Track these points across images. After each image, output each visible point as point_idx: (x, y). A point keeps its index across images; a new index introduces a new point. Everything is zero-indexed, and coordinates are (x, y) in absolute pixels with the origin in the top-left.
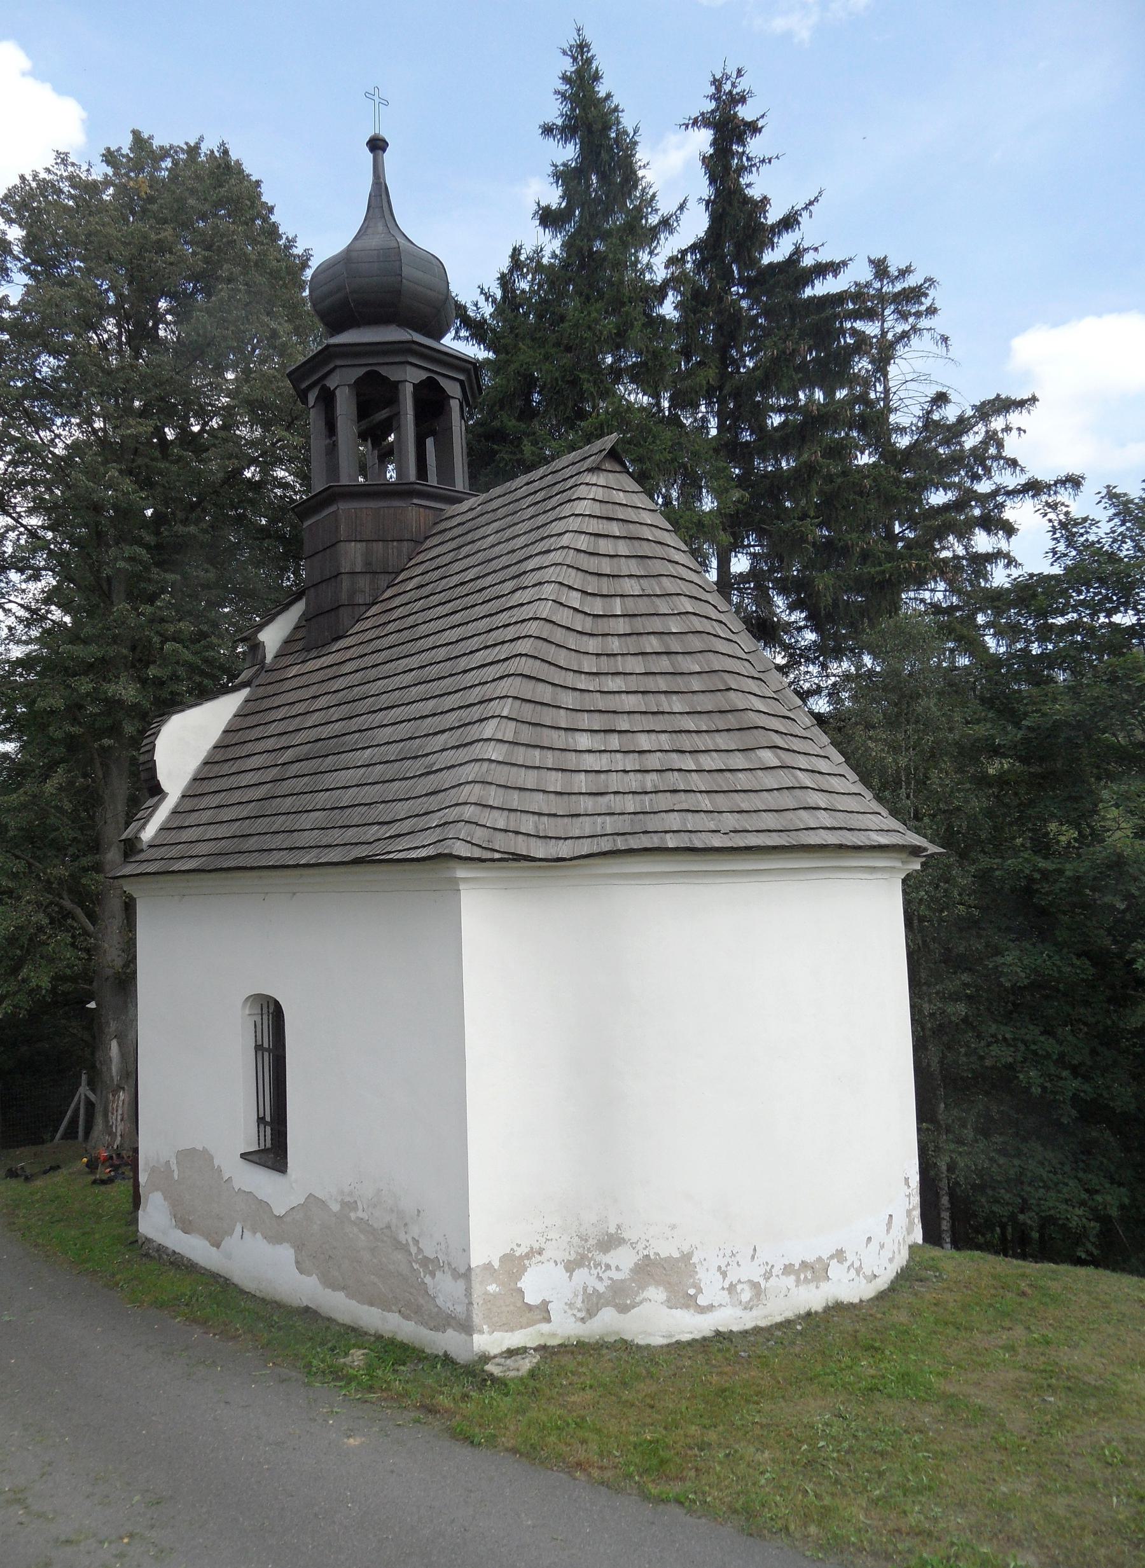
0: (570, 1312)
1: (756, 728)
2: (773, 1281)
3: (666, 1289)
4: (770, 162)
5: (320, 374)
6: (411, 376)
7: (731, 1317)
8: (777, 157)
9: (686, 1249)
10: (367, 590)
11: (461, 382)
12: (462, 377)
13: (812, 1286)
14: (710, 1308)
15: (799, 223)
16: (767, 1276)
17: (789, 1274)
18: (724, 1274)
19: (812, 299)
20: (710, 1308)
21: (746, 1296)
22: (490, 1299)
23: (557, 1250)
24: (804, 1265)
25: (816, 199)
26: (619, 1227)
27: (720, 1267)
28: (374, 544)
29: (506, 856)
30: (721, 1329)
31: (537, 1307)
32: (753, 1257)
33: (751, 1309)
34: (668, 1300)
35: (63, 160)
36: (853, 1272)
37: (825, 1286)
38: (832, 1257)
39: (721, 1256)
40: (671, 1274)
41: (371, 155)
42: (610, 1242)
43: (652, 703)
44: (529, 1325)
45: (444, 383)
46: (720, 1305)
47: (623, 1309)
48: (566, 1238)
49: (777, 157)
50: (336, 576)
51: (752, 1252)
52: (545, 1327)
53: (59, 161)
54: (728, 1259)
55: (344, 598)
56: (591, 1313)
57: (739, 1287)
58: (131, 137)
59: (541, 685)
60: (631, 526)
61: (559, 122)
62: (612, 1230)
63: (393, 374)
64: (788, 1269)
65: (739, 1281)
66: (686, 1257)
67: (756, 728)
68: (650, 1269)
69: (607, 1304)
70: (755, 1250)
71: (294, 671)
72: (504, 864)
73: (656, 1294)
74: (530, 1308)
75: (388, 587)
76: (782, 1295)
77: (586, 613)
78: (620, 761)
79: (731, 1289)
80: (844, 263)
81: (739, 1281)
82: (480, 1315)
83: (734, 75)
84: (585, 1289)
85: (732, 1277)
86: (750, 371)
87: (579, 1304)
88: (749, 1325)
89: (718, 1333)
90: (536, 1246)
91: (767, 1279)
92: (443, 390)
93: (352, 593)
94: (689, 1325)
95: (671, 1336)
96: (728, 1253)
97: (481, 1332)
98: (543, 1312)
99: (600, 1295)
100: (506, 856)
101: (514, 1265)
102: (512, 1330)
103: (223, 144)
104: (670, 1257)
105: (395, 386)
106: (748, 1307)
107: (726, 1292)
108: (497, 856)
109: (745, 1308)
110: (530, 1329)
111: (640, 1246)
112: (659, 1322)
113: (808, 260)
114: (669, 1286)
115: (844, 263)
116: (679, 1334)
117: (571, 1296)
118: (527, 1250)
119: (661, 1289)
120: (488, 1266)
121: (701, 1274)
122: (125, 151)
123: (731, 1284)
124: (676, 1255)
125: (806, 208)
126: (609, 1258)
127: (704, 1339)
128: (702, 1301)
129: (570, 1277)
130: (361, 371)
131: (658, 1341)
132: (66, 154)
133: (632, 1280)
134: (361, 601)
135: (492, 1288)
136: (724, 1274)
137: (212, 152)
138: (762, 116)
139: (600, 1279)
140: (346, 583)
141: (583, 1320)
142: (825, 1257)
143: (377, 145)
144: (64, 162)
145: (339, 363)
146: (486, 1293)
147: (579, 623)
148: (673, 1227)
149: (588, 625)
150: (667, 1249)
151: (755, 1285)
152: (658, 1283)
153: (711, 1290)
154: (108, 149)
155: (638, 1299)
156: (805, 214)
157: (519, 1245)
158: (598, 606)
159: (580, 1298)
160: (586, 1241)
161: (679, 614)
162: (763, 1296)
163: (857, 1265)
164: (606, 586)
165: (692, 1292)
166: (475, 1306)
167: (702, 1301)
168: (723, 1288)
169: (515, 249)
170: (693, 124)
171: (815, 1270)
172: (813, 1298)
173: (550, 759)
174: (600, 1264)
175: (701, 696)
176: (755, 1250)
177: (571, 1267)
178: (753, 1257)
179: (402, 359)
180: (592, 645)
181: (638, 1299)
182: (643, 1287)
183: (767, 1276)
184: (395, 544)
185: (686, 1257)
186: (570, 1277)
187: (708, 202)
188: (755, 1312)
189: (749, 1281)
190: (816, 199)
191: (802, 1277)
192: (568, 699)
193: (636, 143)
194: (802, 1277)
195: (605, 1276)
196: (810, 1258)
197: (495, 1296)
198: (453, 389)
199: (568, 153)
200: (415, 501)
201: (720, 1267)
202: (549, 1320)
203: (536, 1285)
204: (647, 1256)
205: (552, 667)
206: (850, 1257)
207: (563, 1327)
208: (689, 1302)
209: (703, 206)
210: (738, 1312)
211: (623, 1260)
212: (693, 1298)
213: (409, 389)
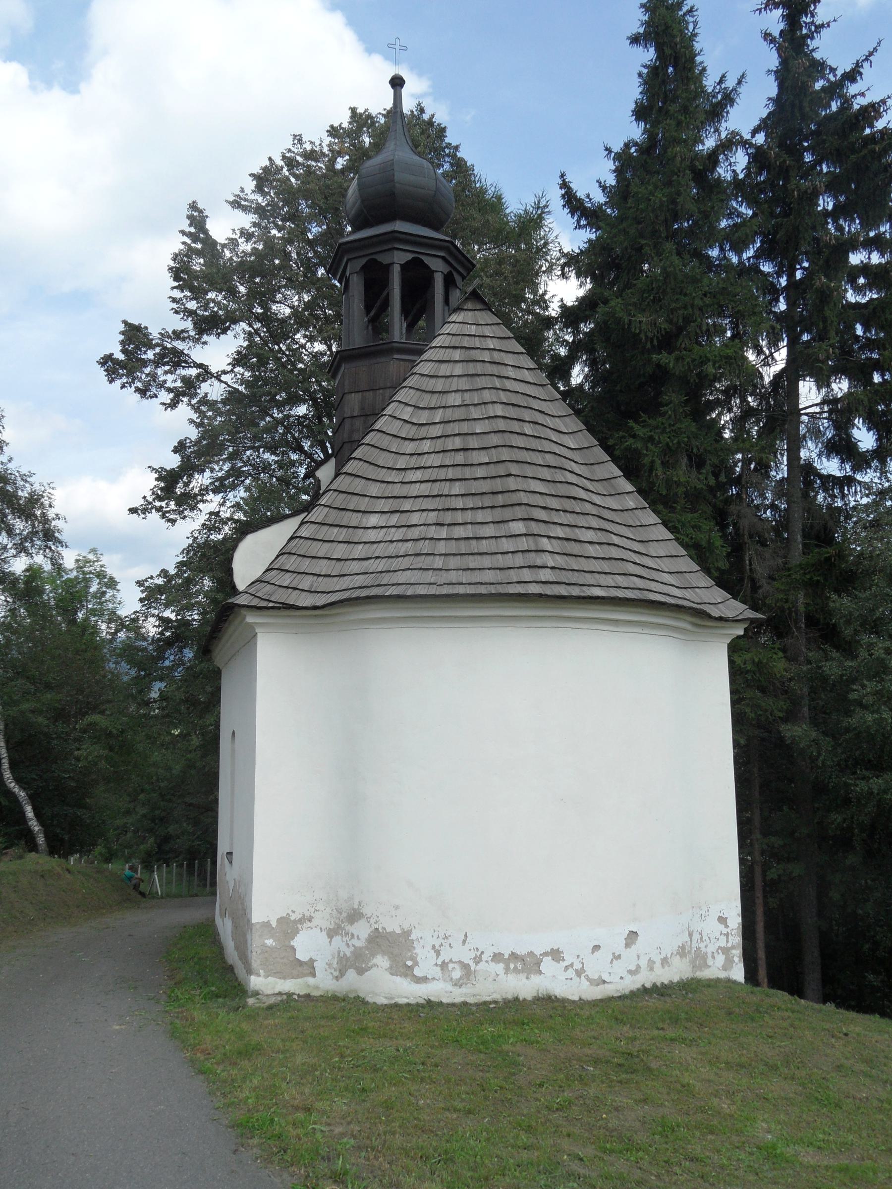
0: (329, 971)
1: (520, 504)
2: (482, 966)
3: (390, 958)
4: (829, 26)
5: (341, 270)
6: (400, 258)
7: (441, 990)
8: (835, 20)
9: (406, 927)
11: (443, 258)
12: (442, 254)
13: (522, 976)
14: (424, 980)
16: (478, 960)
17: (498, 962)
18: (438, 953)
20: (424, 980)
21: (457, 974)
22: (265, 949)
23: (323, 919)
24: (514, 956)
25: (875, 49)
26: (360, 904)
27: (434, 947)
29: (278, 605)
30: (432, 999)
31: (306, 963)
32: (464, 942)
33: (460, 986)
34: (391, 967)
35: (299, 140)
36: (571, 973)
37: (535, 979)
38: (546, 954)
39: (435, 937)
40: (395, 946)
41: (392, 91)
42: (355, 916)
43: (436, 489)
44: (298, 977)
45: (427, 260)
46: (434, 979)
47: (361, 972)
48: (328, 910)
49: (835, 20)
51: (463, 938)
52: (311, 980)
53: (296, 141)
54: (440, 941)
56: (342, 973)
57: (451, 966)
58: (349, 113)
59: (358, 480)
60: (472, 352)
61: (641, 30)
62: (356, 906)
63: (384, 259)
64: (497, 957)
65: (451, 961)
66: (407, 933)
67: (520, 504)
68: (380, 941)
69: (350, 967)
70: (466, 936)
72: (275, 612)
73: (382, 961)
74: (300, 963)
76: (490, 979)
77: (414, 424)
78: (398, 534)
79: (444, 966)
81: (451, 961)
82: (259, 962)
84: (339, 952)
85: (445, 956)
87: (335, 965)
88: (458, 1000)
89: (429, 1002)
90: (307, 914)
91: (477, 963)
92: (427, 267)
94: (406, 991)
95: (392, 998)
96: (442, 935)
97: (258, 975)
98: (309, 968)
99: (347, 959)
100: (278, 605)
101: (289, 927)
102: (284, 978)
103: (419, 104)
104: (394, 932)
105: (388, 268)
106: (457, 984)
107: (439, 968)
108: (271, 605)
109: (456, 985)
110: (299, 980)
111: (372, 921)
112: (385, 985)
114: (393, 957)
116: (398, 997)
117: (330, 958)
118: (301, 916)
119: (386, 957)
120: (267, 925)
121: (418, 950)
122: (345, 125)
123: (444, 962)
124: (398, 931)
125: (867, 59)
126: (354, 929)
127: (418, 1004)
128: (417, 972)
129: (330, 942)
130: (364, 261)
131: (382, 1000)
132: (300, 135)
133: (367, 948)
135: (269, 942)
136: (438, 953)
137: (412, 112)
139: (348, 945)
141: (337, 978)
142: (538, 953)
144: (300, 141)
146: (264, 945)
147: (411, 431)
148: (397, 907)
149: (411, 431)
150: (392, 926)
151: (465, 967)
152: (384, 953)
153: (426, 965)
154: (332, 126)
155: (370, 964)
156: (866, 65)
157: (293, 912)
158: (423, 417)
159: (336, 960)
160: (341, 913)
161: (488, 418)
162: (472, 977)
163: (577, 966)
164: (434, 401)
165: (409, 963)
166: (254, 953)
167: (417, 972)
168: (436, 965)
170: (765, 9)
171: (529, 964)
172: (524, 987)
173: (343, 534)
174: (348, 934)
175: (481, 482)
176: (466, 936)
177: (331, 934)
178: (464, 942)
179: (390, 246)
180: (410, 447)
181: (370, 964)
182: (373, 955)
183: (478, 960)
184: (381, 391)
185: (407, 933)
186: (330, 942)
187: (776, 72)
188: (464, 990)
189: (460, 962)
190: (875, 49)
191: (512, 966)
192: (374, 489)
193: (695, 35)
194: (512, 966)
195: (350, 943)
196: (522, 951)
197: (271, 948)
198: (437, 266)
199: (648, 55)
200: (396, 356)
201: (434, 947)
202: (314, 975)
203: (309, 944)
204: (377, 929)
205: (372, 466)
206: (569, 959)
207: (323, 982)
208: (407, 972)
209: (772, 77)
210: (449, 987)
211: (362, 931)
212: (411, 968)
213: (397, 269)
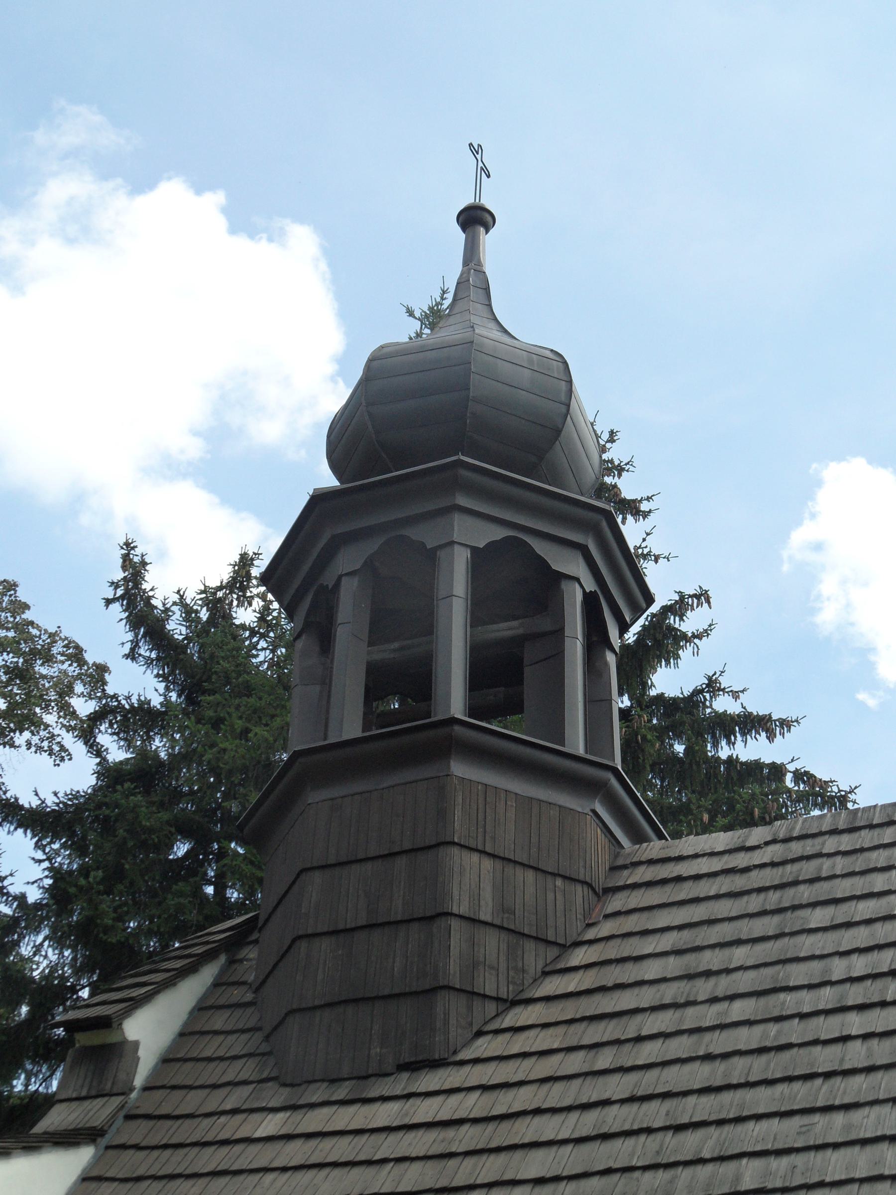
4: (656, 561)
10: (503, 966)
15: (677, 657)
19: (731, 761)
28: (519, 871)
50: (432, 918)
55: (454, 973)
71: (271, 1125)
75: (546, 974)
80: (786, 724)
83: (605, 436)
86: (133, 929)
93: (473, 965)
113: (723, 704)
115: (786, 724)
134: (490, 991)
138: (648, 499)
140: (457, 931)
143: (475, 219)
145: (462, 500)
169: (244, 556)
